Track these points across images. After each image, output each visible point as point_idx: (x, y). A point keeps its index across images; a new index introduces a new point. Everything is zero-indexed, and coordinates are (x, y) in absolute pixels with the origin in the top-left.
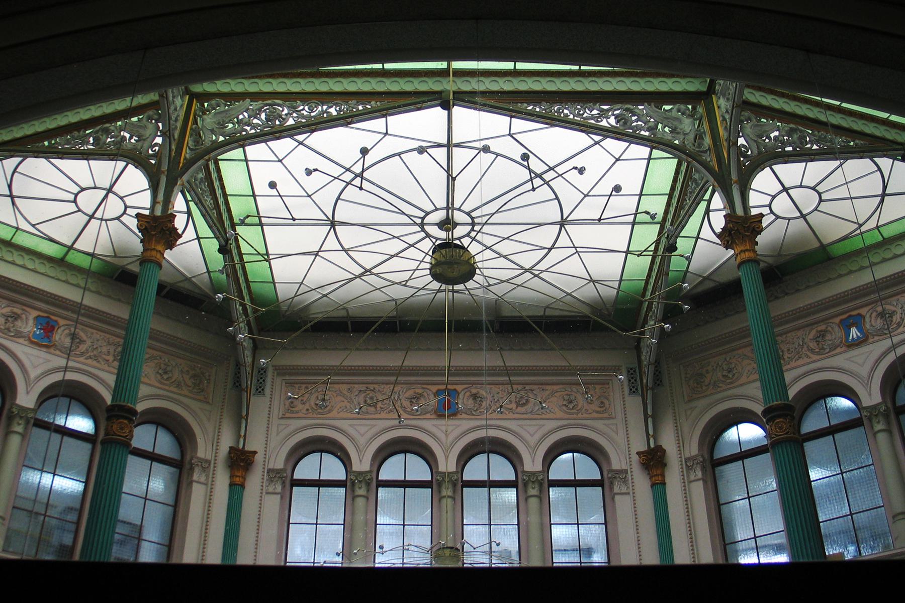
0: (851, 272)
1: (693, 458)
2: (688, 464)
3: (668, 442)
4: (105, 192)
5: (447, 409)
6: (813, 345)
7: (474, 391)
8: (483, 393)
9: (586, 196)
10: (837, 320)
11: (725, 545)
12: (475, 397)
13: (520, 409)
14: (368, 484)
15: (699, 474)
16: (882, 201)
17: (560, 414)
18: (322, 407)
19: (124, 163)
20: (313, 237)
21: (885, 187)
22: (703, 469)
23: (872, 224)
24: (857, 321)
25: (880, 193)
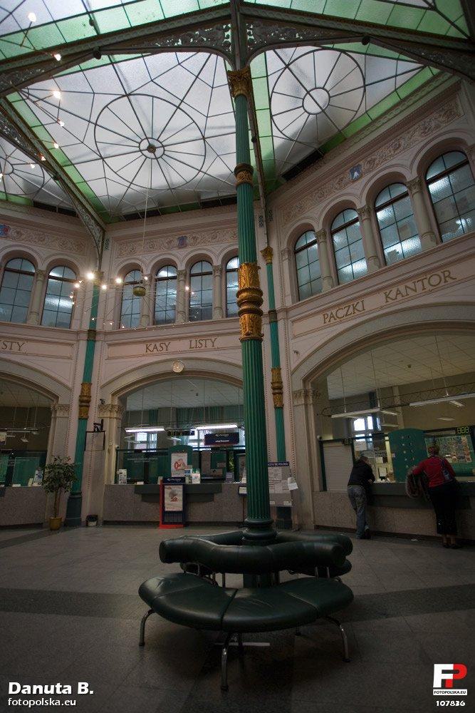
0: (355, 143)
1: (284, 250)
2: (282, 254)
3: (274, 245)
4: (269, 74)
5: (182, 243)
6: (337, 186)
7: (369, 159)
8: (197, 236)
9: (94, 93)
10: (177, 237)
11: (334, 252)
12: (194, 238)
13: (214, 241)
14: (185, 276)
15: (287, 257)
16: (365, 91)
17: (230, 240)
18: (133, 251)
19: (209, 54)
20: (80, 127)
21: (123, 96)
22: (289, 254)
23: (362, 110)
24: (357, 168)
25: (362, 85)
